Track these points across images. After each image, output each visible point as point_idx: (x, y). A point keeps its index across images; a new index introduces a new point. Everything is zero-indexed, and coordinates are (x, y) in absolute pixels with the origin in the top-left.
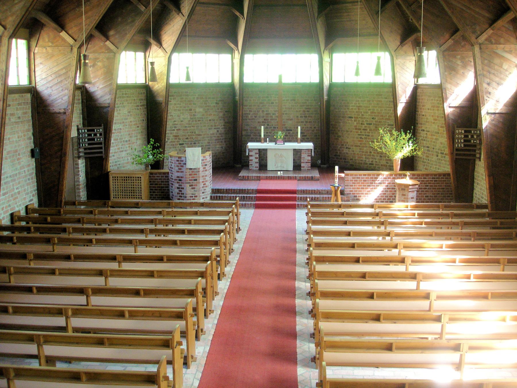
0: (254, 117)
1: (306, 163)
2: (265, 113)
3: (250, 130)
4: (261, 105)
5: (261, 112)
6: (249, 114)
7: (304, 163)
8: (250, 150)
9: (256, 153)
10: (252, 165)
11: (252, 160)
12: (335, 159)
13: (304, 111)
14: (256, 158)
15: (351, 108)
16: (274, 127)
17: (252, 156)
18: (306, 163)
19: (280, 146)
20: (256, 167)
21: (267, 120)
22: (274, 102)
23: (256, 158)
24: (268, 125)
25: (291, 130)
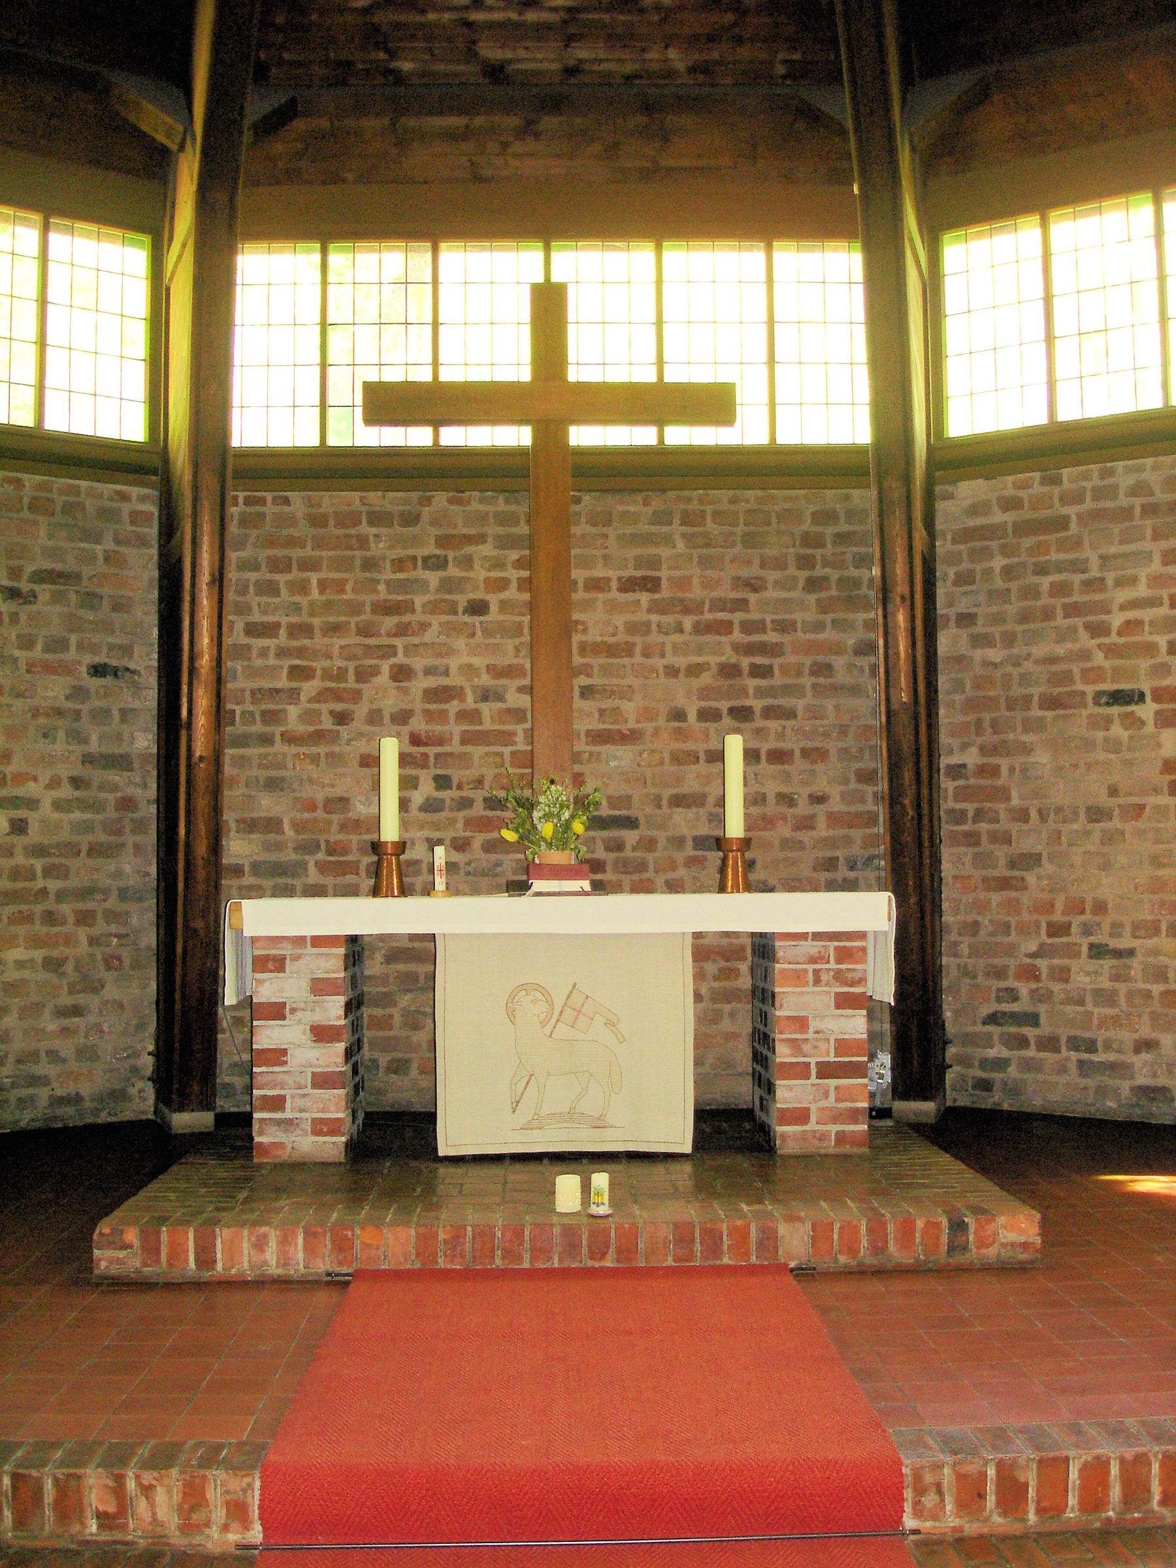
0: (327, 723)
1: (826, 1070)
2: (422, 683)
3: (298, 827)
4: (390, 622)
5: (384, 678)
6: (293, 695)
7: (801, 1071)
8: (270, 961)
9: (320, 987)
10: (277, 1103)
11: (278, 1056)
12: (997, 1051)
13: (729, 671)
14: (321, 1034)
15: (1117, 620)
16: (493, 803)
17: (277, 1012)
18: (826, 1070)
19: (561, 911)
20: (321, 1127)
21: (440, 741)
22: (494, 600)
23: (321, 1034)
24: (442, 782)
25: (631, 823)
